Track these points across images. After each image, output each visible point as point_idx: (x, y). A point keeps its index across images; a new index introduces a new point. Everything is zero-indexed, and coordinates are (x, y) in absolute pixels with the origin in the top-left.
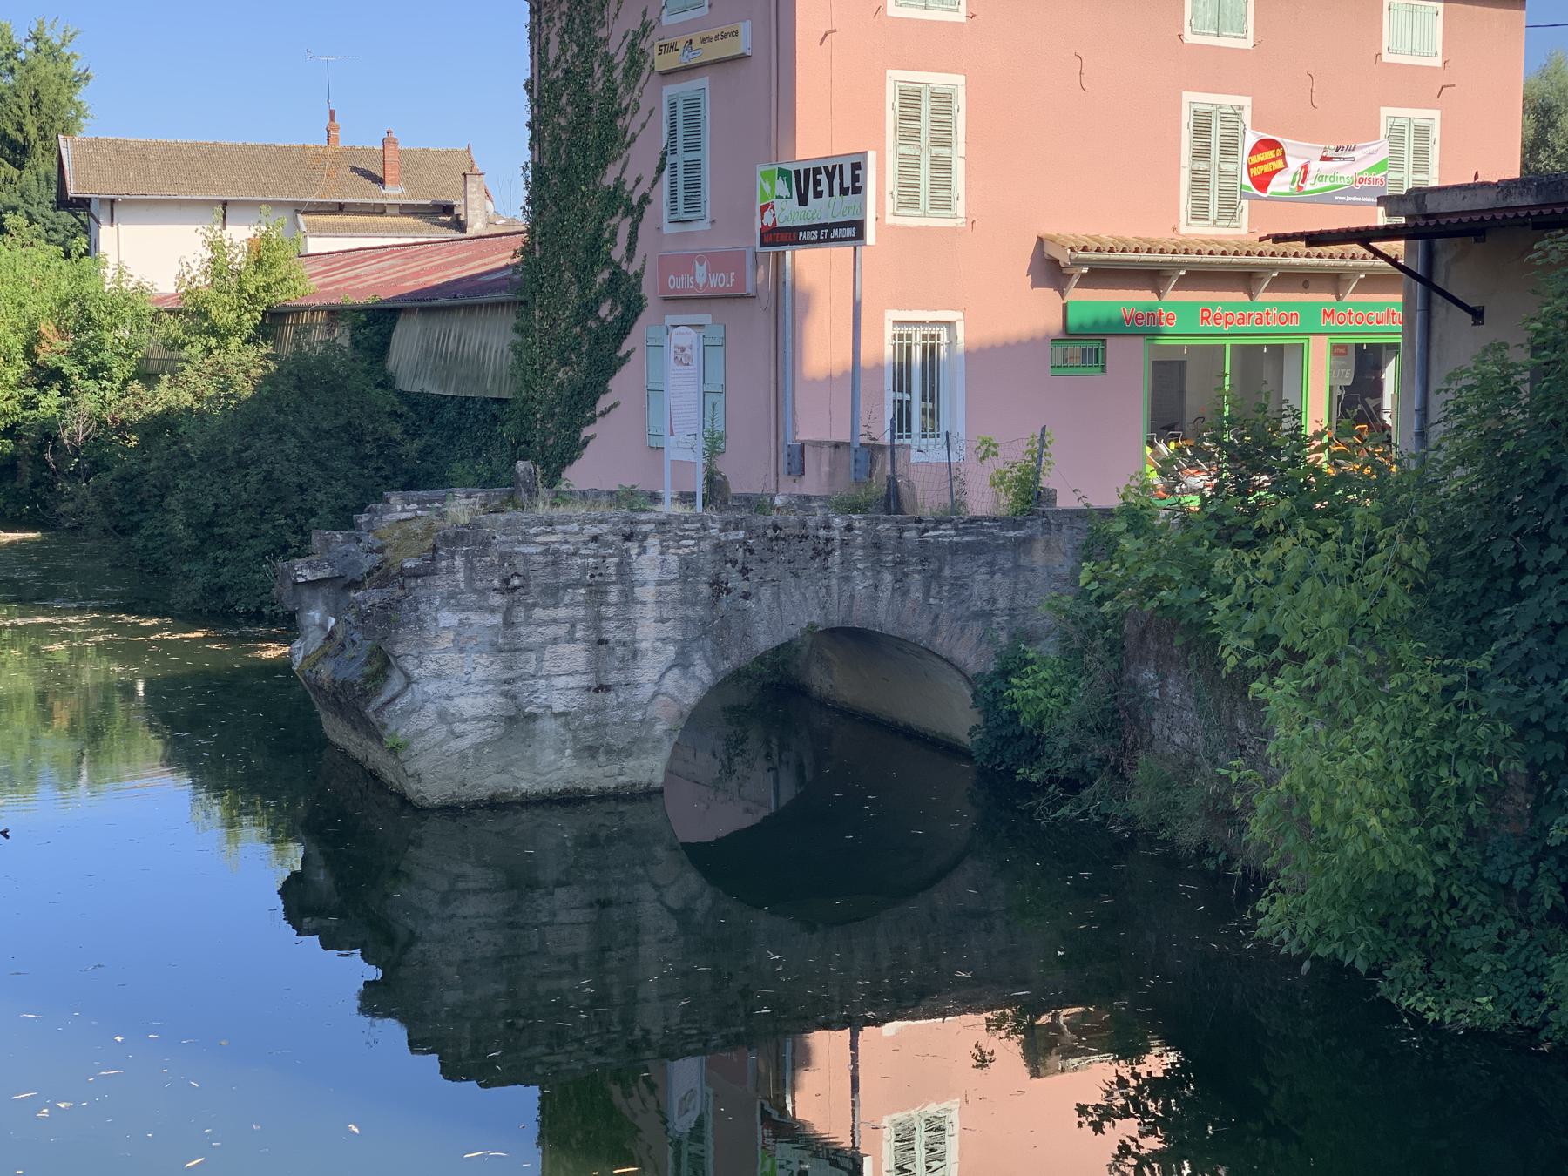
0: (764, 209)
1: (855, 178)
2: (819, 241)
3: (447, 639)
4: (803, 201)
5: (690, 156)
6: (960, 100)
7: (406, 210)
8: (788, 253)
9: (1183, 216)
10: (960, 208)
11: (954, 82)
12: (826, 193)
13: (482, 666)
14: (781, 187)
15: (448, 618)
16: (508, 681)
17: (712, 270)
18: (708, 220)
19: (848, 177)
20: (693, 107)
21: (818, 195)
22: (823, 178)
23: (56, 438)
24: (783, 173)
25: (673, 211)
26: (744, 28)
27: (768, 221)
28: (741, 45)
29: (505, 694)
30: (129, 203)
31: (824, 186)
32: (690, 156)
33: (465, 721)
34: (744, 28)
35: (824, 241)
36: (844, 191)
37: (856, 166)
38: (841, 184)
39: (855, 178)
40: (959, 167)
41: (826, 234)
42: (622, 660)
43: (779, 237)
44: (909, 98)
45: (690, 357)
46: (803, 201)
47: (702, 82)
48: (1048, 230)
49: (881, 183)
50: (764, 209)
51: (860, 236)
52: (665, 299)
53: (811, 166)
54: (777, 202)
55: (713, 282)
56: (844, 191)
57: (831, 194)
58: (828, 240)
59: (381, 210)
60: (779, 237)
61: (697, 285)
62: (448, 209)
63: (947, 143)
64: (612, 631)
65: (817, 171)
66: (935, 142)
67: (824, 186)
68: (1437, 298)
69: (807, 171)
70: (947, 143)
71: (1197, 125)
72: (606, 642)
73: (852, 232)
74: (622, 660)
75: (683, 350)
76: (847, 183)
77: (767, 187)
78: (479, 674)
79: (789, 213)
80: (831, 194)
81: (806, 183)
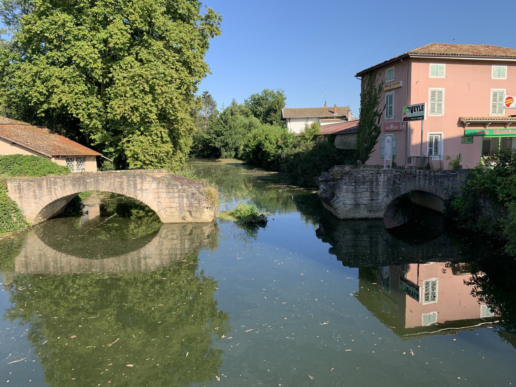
1: (422, 108)
4: (412, 112)
6: (444, 93)
7: (337, 117)
9: (491, 112)
10: (443, 112)
11: (443, 89)
15: (345, 187)
19: (421, 107)
20: (391, 96)
21: (415, 111)
22: (416, 108)
24: (408, 108)
26: (401, 82)
27: (405, 116)
28: (401, 85)
31: (416, 110)
34: (401, 82)
36: (420, 110)
37: (423, 106)
39: (422, 108)
40: (443, 105)
41: (416, 118)
44: (433, 93)
46: (412, 112)
47: (393, 92)
58: (417, 119)
59: (333, 118)
63: (441, 101)
64: (374, 190)
66: (438, 100)
70: (441, 101)
73: (421, 118)
76: (421, 109)
78: (350, 197)
79: (409, 115)
81: (413, 109)
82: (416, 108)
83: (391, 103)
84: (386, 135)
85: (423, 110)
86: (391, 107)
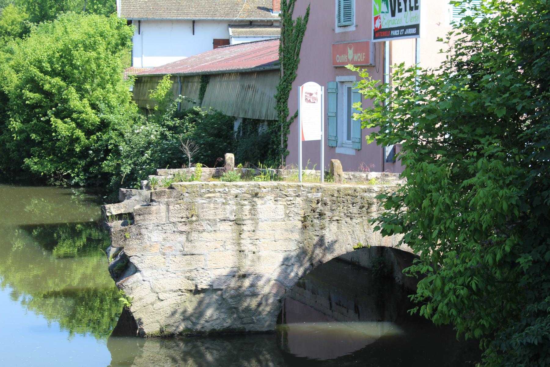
0: (376, 19)
2: (399, 36)
4: (393, 15)
8: (387, 43)
12: (403, 10)
16: (191, 271)
17: (355, 52)
18: (354, 25)
21: (400, 11)
23: (430, 111)
27: (378, 25)
30: (149, 21)
31: (403, 6)
33: (165, 292)
36: (411, 9)
38: (410, 5)
42: (253, 261)
43: (383, 33)
45: (316, 99)
46: (393, 15)
50: (376, 19)
51: (417, 33)
52: (336, 68)
54: (382, 16)
56: (411, 9)
57: (406, 10)
60: (383, 33)
67: (403, 6)
68: (275, 81)
72: (243, 251)
73: (414, 31)
75: (311, 94)
76: (413, 4)
77: (377, 8)
79: (387, 21)
80: (406, 10)
84: (339, 79)
85: (417, 8)
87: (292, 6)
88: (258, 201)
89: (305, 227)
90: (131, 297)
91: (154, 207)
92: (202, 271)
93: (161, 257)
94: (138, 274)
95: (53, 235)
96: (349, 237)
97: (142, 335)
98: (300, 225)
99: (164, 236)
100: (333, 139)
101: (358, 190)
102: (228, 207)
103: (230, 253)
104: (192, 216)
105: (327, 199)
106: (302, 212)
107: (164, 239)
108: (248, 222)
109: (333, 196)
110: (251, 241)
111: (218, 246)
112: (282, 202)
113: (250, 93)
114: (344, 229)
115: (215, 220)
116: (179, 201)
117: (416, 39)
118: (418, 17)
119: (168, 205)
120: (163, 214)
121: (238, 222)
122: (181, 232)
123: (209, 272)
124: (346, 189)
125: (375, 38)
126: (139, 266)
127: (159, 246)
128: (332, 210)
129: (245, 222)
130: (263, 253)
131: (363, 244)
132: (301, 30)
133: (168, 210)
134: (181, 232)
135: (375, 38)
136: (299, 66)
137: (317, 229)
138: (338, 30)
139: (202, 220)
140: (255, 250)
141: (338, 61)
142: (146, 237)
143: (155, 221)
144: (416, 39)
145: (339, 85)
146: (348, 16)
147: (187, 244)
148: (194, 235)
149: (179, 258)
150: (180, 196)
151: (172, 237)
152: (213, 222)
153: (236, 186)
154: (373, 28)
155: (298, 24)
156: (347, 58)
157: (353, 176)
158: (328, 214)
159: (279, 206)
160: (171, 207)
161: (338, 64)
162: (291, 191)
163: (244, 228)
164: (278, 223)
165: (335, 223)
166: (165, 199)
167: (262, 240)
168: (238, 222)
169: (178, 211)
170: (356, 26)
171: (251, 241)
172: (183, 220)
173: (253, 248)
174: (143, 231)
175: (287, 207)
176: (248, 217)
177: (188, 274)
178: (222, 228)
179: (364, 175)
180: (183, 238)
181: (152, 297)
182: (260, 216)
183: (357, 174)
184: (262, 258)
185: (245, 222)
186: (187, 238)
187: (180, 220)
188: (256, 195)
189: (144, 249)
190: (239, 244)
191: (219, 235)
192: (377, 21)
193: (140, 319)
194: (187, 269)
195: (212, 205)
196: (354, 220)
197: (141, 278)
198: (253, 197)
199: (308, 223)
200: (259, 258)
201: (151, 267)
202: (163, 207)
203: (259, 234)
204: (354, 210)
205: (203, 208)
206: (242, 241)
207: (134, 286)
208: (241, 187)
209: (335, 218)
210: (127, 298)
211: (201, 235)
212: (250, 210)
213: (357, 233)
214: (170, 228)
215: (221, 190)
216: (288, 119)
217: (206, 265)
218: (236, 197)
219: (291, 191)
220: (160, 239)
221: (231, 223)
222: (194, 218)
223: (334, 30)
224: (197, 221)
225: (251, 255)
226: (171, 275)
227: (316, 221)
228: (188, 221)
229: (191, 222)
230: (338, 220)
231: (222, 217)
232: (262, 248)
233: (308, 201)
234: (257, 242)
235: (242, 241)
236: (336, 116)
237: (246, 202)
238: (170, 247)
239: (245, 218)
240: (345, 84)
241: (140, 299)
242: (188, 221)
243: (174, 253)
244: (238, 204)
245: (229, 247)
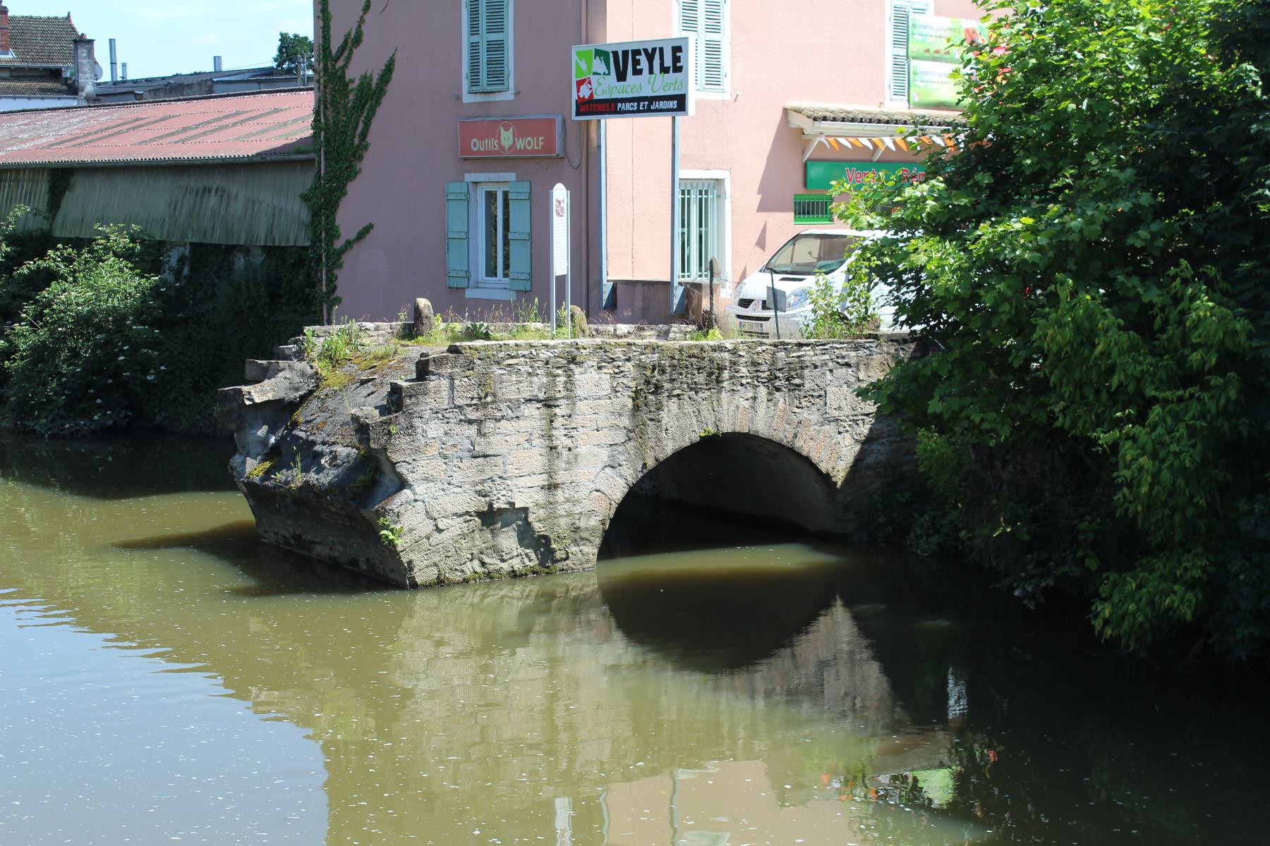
0: (580, 83)
1: (676, 59)
2: (638, 111)
3: (433, 451)
4: (621, 77)
5: (493, 37)
8: (603, 121)
12: (646, 70)
13: (467, 471)
14: (599, 65)
15: (434, 429)
16: (483, 482)
21: (637, 72)
22: (643, 58)
24: (599, 53)
25: (474, 82)
27: (585, 92)
29: (479, 493)
32: (493, 37)
35: (644, 111)
36: (664, 70)
37: (677, 50)
39: (676, 59)
41: (646, 105)
42: (568, 462)
46: (621, 77)
48: (792, 104)
49: (695, 60)
50: (580, 83)
53: (630, 48)
54: (594, 79)
55: (520, 144)
57: (651, 72)
58: (648, 110)
61: (502, 148)
62: (55, 74)
64: (561, 441)
65: (636, 52)
69: (625, 53)
71: (897, 18)
73: (673, 104)
74: (568, 462)
76: (668, 62)
77: (583, 66)
78: (458, 477)
79: (606, 87)
80: (651, 72)
81: (625, 62)
82: (643, 58)
83: (497, 25)
84: (469, 177)
85: (678, 69)
86: (497, 47)
87: (346, 54)
88: (577, 370)
89: (636, 408)
90: (398, 527)
91: (433, 383)
92: (499, 481)
93: (441, 461)
94: (406, 493)
95: (1217, 362)
96: (694, 420)
97: (415, 586)
98: (630, 403)
99: (446, 427)
100: (463, 274)
101: (707, 348)
102: (535, 379)
103: (537, 451)
104: (486, 395)
105: (666, 363)
106: (633, 384)
107: (446, 434)
108: (562, 402)
109: (673, 358)
110: (565, 432)
111: (522, 440)
112: (609, 369)
113: (213, 200)
114: (688, 409)
115: (518, 400)
116: (468, 373)
117: (674, 118)
118: (685, 83)
119: (452, 379)
120: (445, 394)
121: (548, 403)
122: (470, 422)
123: (509, 482)
124: (690, 347)
125: (578, 114)
126: (410, 477)
127: (438, 445)
128: (672, 380)
129: (558, 403)
130: (583, 450)
131: (712, 430)
132: (371, 94)
133: (452, 387)
134: (470, 422)
135: (578, 114)
136: (365, 154)
137: (653, 409)
138: (467, 98)
139: (501, 401)
140: (571, 445)
141: (475, 149)
142: (419, 431)
143: (433, 405)
144: (674, 118)
145: (471, 186)
146: (497, 74)
147: (478, 439)
148: (489, 426)
149: (467, 462)
150: (470, 365)
151: (457, 429)
152: (515, 405)
153: (546, 346)
154: (575, 97)
155: (362, 84)
156: (499, 143)
157: (597, 330)
158: (667, 386)
159: (603, 376)
160: (457, 382)
161: (474, 153)
162: (618, 353)
163: (557, 411)
164: (602, 402)
165: (675, 399)
166: (447, 370)
167: (581, 429)
168: (548, 403)
169: (466, 391)
170: (517, 93)
171: (565, 432)
172: (474, 402)
173: (568, 442)
174: (417, 422)
175: (613, 376)
176: (563, 394)
177: (479, 488)
178: (527, 413)
179: (610, 328)
180: (472, 430)
181: (428, 527)
182: (579, 392)
183: (601, 327)
184: (580, 458)
185: (558, 403)
186: (479, 431)
187: (469, 402)
188: (573, 360)
189: (417, 450)
190: (550, 437)
191: (522, 424)
192: (583, 88)
193: (410, 562)
194: (477, 479)
195: (514, 378)
196: (700, 394)
197: (412, 497)
198: (569, 362)
199: (641, 401)
200: (576, 457)
201: (426, 480)
202: (445, 383)
203: (577, 420)
204: (701, 378)
205: (501, 382)
206: (554, 432)
207: (402, 510)
208: (554, 347)
209: (675, 392)
210: (392, 530)
211: (498, 424)
212: (566, 383)
213: (704, 413)
214: (454, 416)
215: (526, 353)
216: (338, 244)
217: (505, 472)
218: (547, 363)
219: (618, 353)
220: (441, 433)
221: (539, 405)
222: (489, 399)
223: (459, 98)
224: (493, 402)
225: (565, 453)
226: (456, 490)
227: (651, 397)
228: (481, 404)
229: (485, 405)
230: (678, 395)
231: (527, 395)
232: (580, 442)
233: (641, 366)
234: (574, 433)
235: (554, 432)
236: (467, 238)
237: (560, 372)
238: (454, 446)
239: (558, 395)
240: (479, 188)
241: (411, 530)
242: (481, 404)
243: (460, 454)
244: (549, 374)
245: (536, 442)
